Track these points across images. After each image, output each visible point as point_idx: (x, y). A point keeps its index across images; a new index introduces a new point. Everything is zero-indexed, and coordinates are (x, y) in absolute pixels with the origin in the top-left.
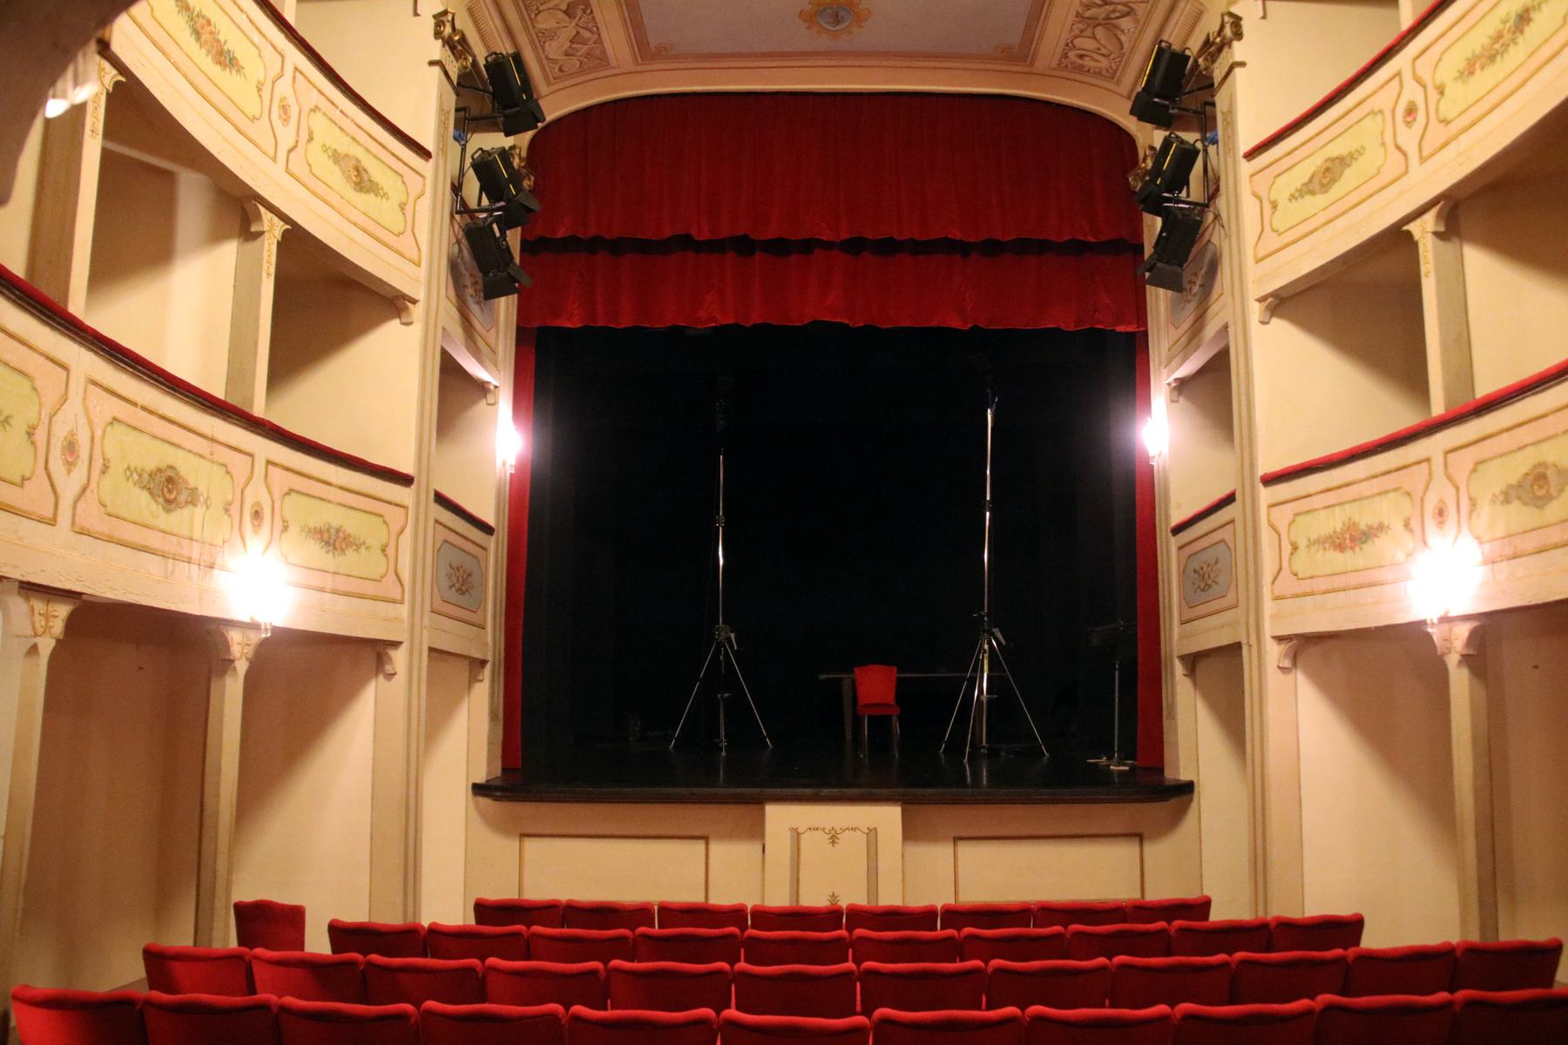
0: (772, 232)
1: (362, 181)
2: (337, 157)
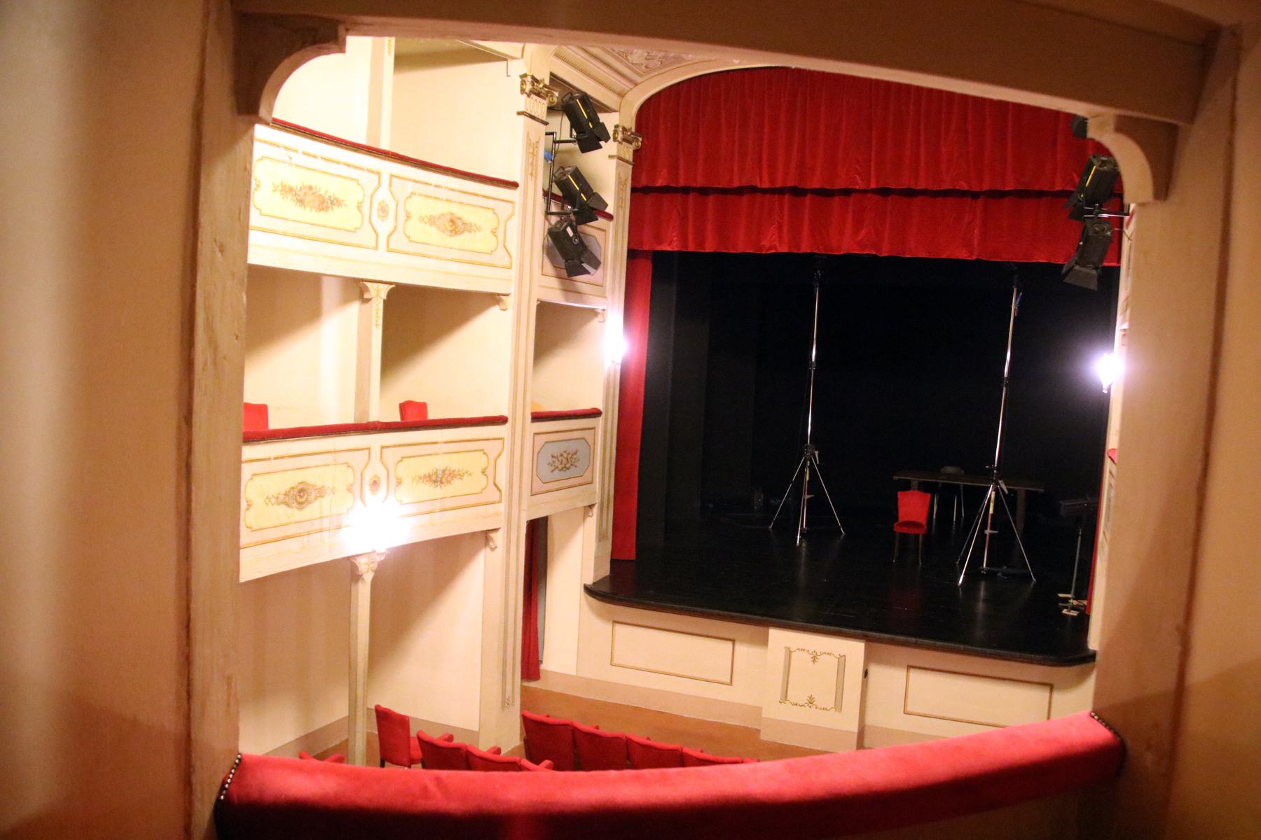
1: (456, 226)
2: (432, 221)
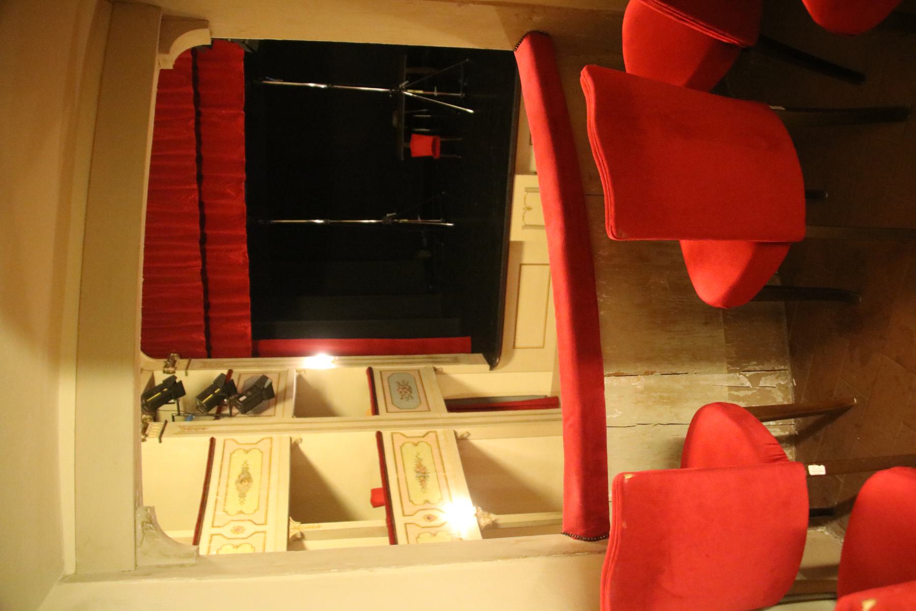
0: (196, 227)
1: (245, 478)
2: (242, 496)
